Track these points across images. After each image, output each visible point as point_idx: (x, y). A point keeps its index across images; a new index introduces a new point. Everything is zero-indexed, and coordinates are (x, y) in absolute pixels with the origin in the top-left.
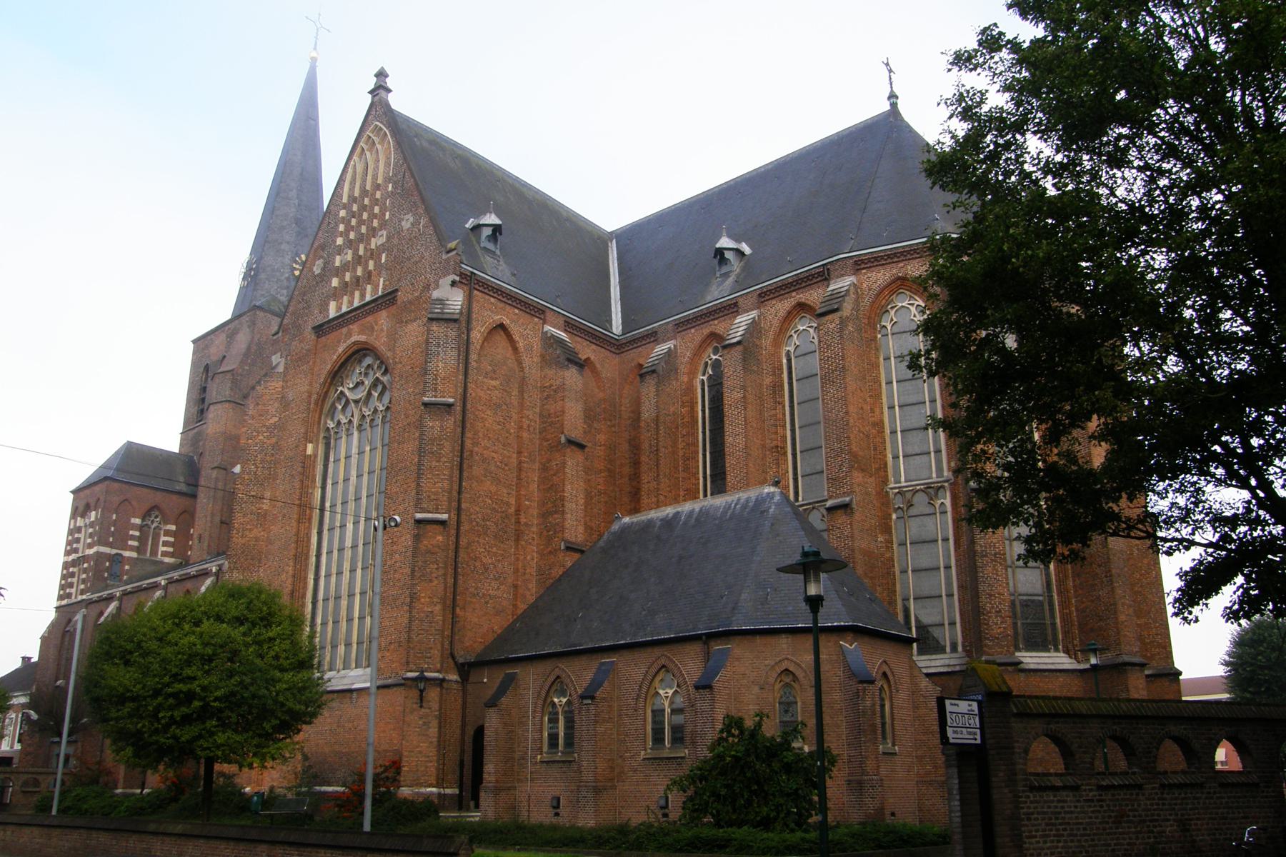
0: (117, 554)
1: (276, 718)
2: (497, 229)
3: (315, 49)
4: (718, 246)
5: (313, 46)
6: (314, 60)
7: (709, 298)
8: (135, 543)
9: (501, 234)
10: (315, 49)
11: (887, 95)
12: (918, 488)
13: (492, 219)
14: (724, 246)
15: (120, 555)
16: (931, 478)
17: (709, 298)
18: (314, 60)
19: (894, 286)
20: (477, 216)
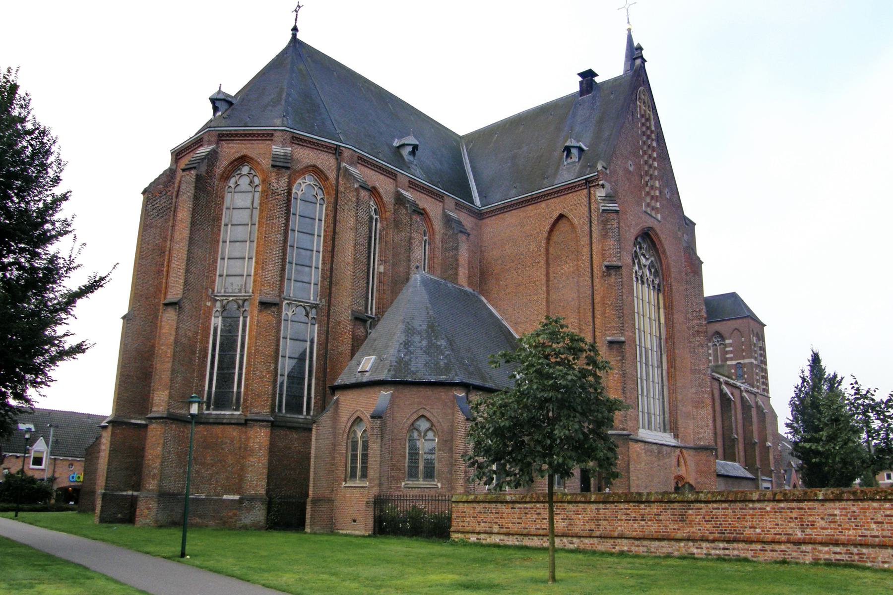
0: (737, 363)
1: (162, 406)
2: (415, 147)
3: (629, 22)
4: (566, 145)
5: (627, 21)
6: (629, 30)
7: (556, 182)
8: (728, 356)
9: (417, 150)
10: (629, 22)
11: (292, 27)
12: (231, 298)
13: (411, 140)
14: (572, 145)
15: (740, 363)
16: (310, 300)
17: (556, 182)
18: (629, 30)
19: (311, 169)
20: (400, 138)
